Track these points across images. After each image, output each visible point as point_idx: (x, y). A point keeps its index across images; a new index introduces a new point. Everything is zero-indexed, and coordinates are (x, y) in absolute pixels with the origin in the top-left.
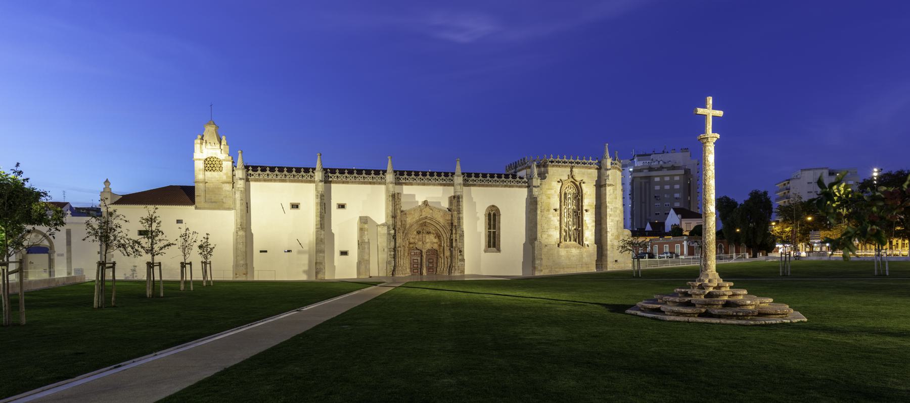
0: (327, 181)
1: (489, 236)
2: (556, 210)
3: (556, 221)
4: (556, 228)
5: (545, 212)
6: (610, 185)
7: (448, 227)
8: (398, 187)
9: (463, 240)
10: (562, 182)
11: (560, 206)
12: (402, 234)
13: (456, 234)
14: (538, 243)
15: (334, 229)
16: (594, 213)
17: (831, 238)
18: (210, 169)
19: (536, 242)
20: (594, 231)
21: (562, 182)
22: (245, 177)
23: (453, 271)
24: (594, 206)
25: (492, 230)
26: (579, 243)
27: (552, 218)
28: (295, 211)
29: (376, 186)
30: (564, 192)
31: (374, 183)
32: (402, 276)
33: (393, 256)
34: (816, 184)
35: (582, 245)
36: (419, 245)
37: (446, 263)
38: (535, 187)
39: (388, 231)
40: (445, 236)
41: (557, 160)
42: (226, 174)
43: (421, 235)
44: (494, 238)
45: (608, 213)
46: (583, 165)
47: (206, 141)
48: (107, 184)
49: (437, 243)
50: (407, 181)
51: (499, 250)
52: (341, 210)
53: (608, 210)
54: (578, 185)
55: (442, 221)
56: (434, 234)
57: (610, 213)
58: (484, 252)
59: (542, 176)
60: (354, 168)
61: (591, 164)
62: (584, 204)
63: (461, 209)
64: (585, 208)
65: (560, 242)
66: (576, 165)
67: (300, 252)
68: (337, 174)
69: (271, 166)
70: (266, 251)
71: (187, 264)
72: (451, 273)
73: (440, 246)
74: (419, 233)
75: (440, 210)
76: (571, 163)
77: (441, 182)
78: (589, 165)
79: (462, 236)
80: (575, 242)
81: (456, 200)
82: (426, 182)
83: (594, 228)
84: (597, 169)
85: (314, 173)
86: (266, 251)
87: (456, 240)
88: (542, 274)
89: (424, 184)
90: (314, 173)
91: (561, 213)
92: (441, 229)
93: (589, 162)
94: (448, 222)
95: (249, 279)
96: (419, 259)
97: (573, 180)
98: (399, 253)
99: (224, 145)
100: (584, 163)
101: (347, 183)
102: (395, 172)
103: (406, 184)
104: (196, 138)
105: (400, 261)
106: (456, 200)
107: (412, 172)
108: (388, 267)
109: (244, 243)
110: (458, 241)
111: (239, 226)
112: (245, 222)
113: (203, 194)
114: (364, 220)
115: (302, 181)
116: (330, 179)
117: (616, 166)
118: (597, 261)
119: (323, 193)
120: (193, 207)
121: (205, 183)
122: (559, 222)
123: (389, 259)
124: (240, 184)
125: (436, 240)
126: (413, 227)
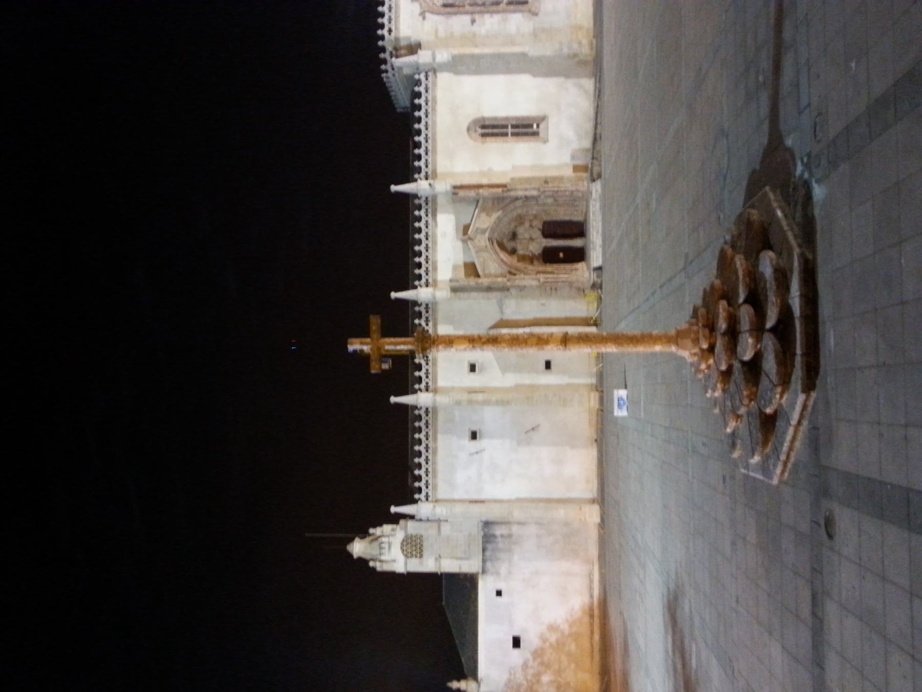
2: (473, 21)
8: (440, 285)
51: (543, 118)
90: (421, 408)
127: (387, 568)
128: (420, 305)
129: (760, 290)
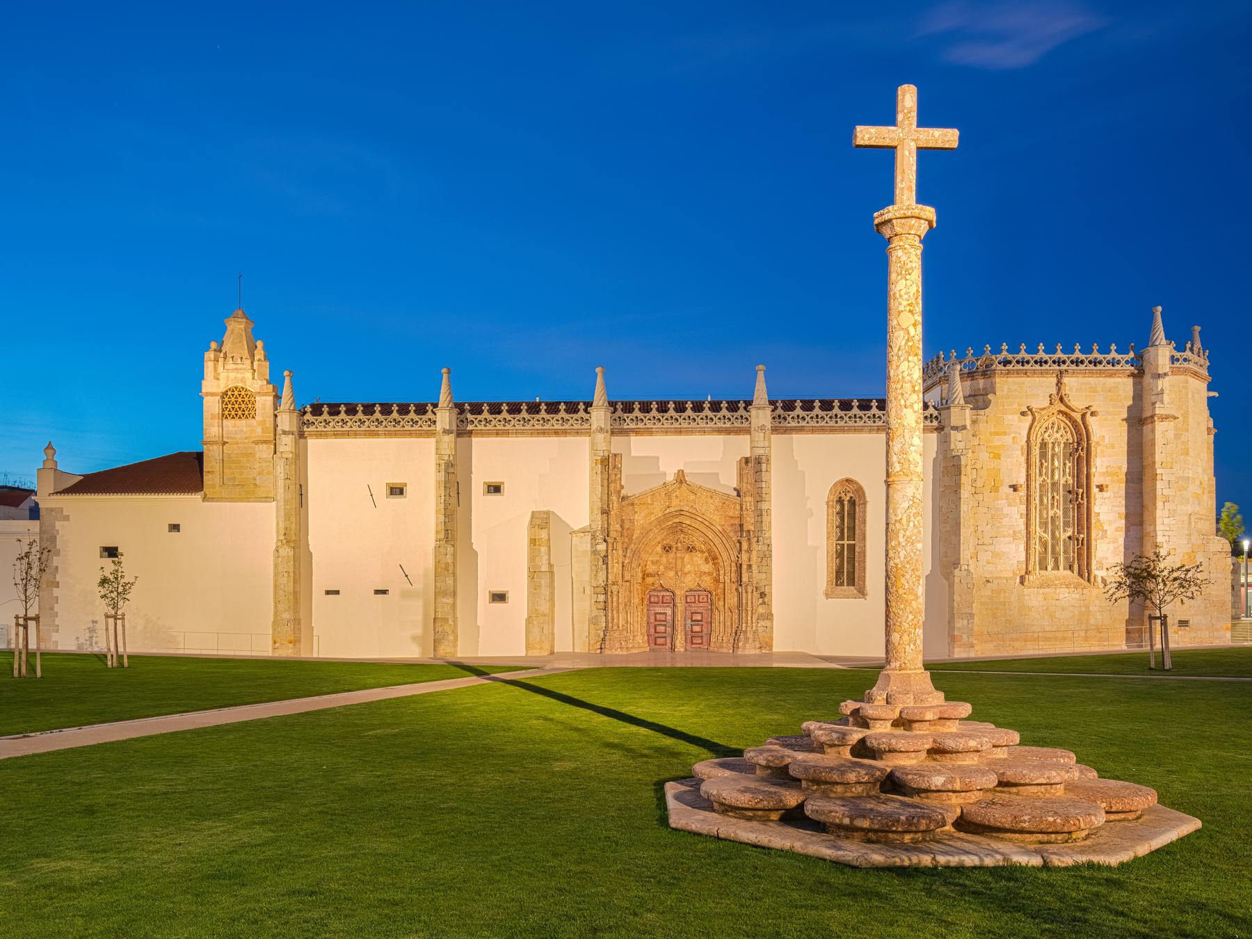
0: (462, 432)
1: (840, 555)
2: (1015, 488)
3: (1018, 516)
4: (1015, 536)
5: (987, 493)
6: (1165, 418)
7: (731, 534)
9: (769, 566)
10: (1033, 414)
11: (1028, 476)
12: (621, 552)
13: (749, 551)
14: (964, 573)
15: (479, 541)
16: (1123, 493)
18: (233, 413)
19: (957, 572)
20: (1121, 541)
21: (1033, 414)
22: (295, 429)
23: (740, 644)
24: (1124, 477)
25: (846, 542)
26: (1081, 575)
27: (1006, 510)
28: (397, 500)
29: (569, 439)
30: (1039, 440)
31: (565, 433)
32: (619, 652)
33: (602, 604)
34: (205, 378)
35: (1089, 580)
36: (669, 579)
37: (728, 620)
38: (955, 428)
39: (592, 547)
40: (727, 558)
41: (1019, 357)
42: (263, 423)
43: (671, 555)
44: (852, 560)
45: (1159, 492)
46: (1092, 367)
47: (225, 354)
48: (50, 451)
49: (710, 574)
50: (641, 425)
52: (494, 498)
53: (1159, 485)
54: (1079, 420)
55: (717, 520)
56: (702, 552)
57: (1166, 492)
58: (824, 597)
59: (979, 400)
60: (538, 400)
61: (1113, 363)
62: (1093, 470)
63: (764, 491)
64: (1095, 481)
65: (1027, 572)
66: (1074, 367)
67: (405, 595)
68: (486, 415)
69: (365, 402)
70: (337, 592)
71: (31, 619)
72: (738, 648)
73: (717, 580)
74: (668, 549)
75: (713, 493)
76: (1059, 362)
77: (720, 425)
78: (1110, 367)
79: (766, 556)
80: (1069, 572)
81: (754, 466)
82: (702, 424)
83: (1123, 534)
84: (1132, 375)
85: (435, 414)
86: (337, 592)
87: (750, 566)
88: (973, 654)
89: (679, 432)
91: (1028, 496)
92: (717, 541)
93: (1109, 357)
94: (732, 521)
95: (304, 654)
96: (669, 612)
97: (1063, 408)
98: (615, 599)
99: (259, 360)
100: (1096, 363)
101: (506, 433)
102: (612, 404)
103: (637, 432)
104: (208, 349)
105: (615, 616)
106: (754, 466)
107: (322, 405)
108: (593, 632)
109: (292, 574)
110: (754, 567)
111: (282, 537)
112: (293, 526)
113: (217, 468)
114: (542, 521)
115: (410, 434)
116: (470, 427)
117: (1186, 365)
118: (1128, 622)
119: (451, 458)
120: (197, 497)
121: (225, 443)
122: (1024, 520)
123: (595, 612)
124: (286, 444)
125: (707, 568)
126: (651, 535)
127: (209, 366)
128: (586, 411)
129: (917, 853)
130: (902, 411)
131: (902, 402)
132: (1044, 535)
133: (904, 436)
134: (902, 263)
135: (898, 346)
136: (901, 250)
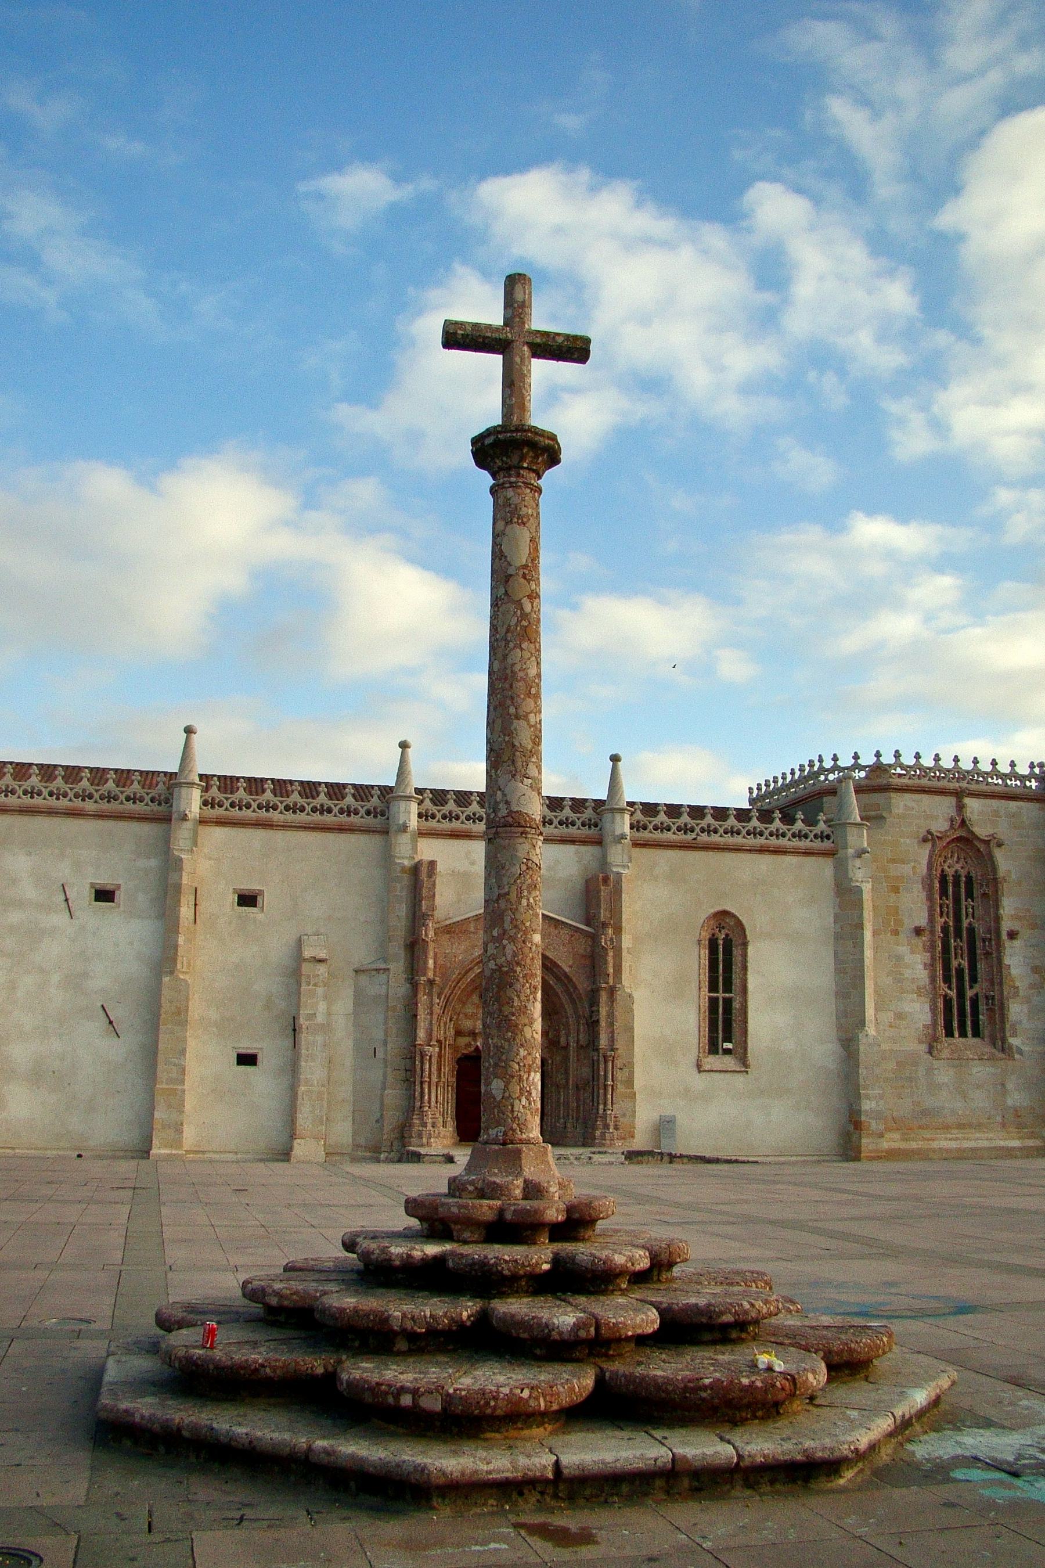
3: (921, 967)
17: (733, 1023)
25: (721, 995)
64: (1006, 926)
98: (427, 1066)
130: (512, 723)
131: (512, 710)
132: (949, 992)
133: (513, 762)
134: (513, 506)
135: (505, 627)
136: (511, 489)
